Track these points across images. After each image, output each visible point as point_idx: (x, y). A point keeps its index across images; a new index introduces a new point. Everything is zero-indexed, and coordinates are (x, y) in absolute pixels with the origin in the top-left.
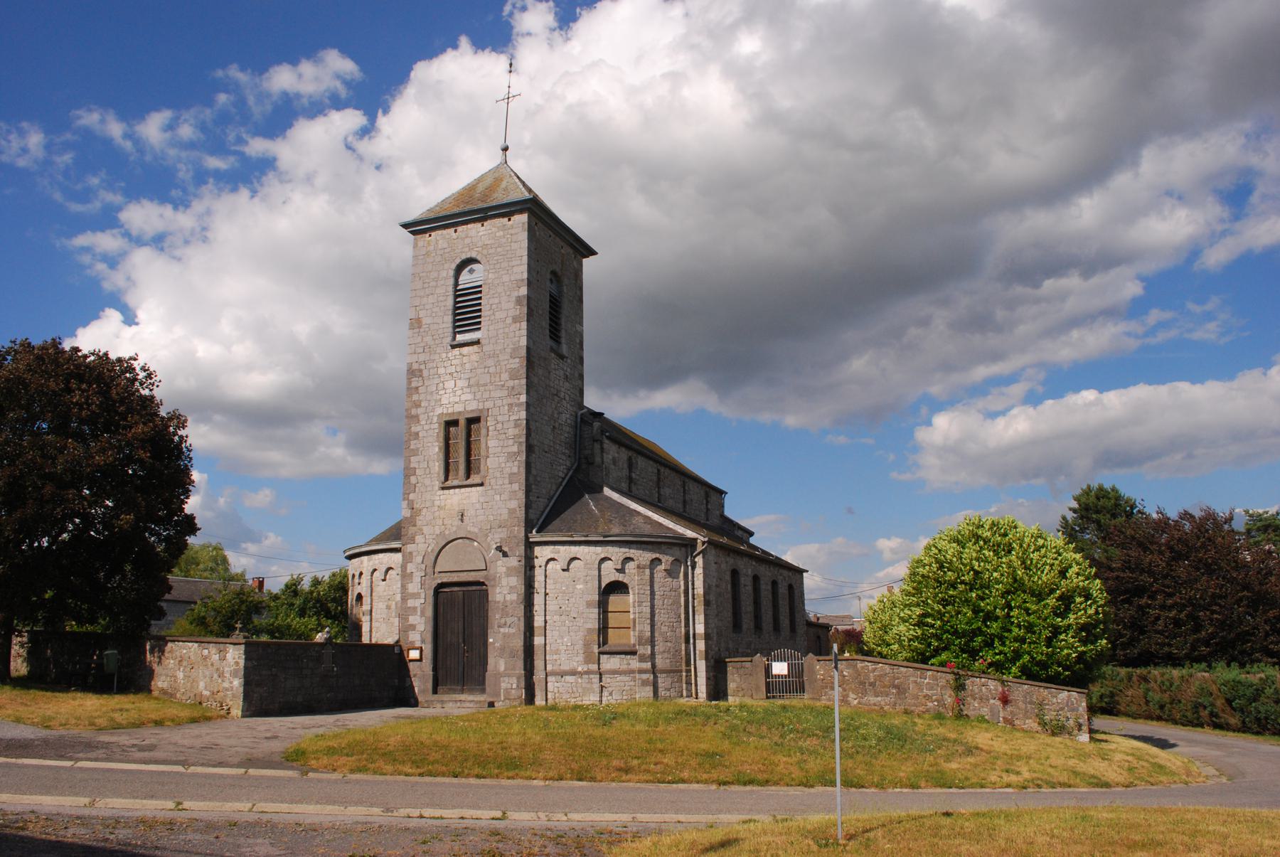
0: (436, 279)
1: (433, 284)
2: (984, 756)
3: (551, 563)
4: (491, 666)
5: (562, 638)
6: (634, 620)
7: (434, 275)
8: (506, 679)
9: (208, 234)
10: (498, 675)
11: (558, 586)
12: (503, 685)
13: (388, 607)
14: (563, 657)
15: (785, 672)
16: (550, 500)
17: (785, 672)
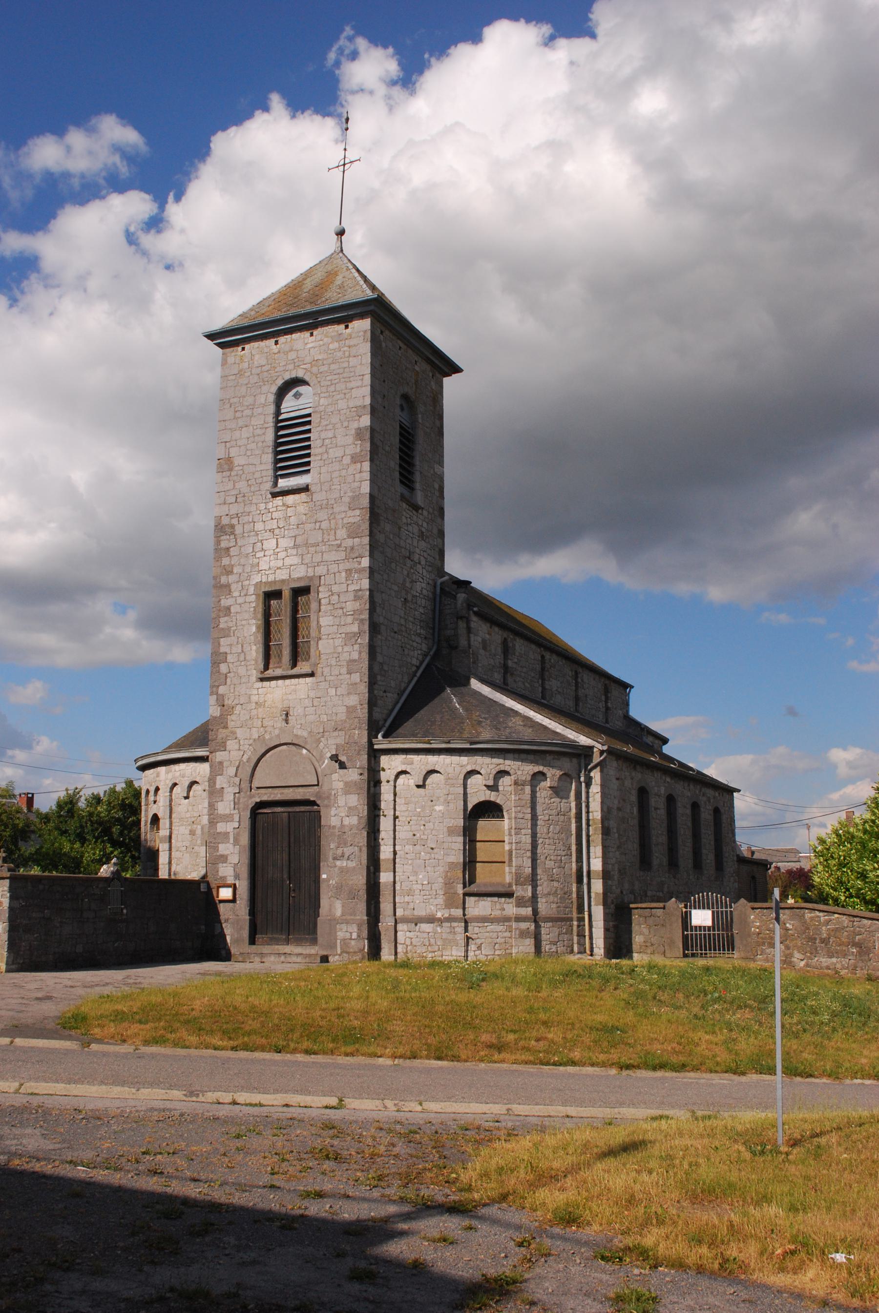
1: (248, 412)
5: (416, 873)
6: (510, 852)
7: (249, 400)
8: (344, 926)
11: (411, 807)
12: (340, 935)
13: (192, 833)
15: (709, 923)
17: (709, 923)
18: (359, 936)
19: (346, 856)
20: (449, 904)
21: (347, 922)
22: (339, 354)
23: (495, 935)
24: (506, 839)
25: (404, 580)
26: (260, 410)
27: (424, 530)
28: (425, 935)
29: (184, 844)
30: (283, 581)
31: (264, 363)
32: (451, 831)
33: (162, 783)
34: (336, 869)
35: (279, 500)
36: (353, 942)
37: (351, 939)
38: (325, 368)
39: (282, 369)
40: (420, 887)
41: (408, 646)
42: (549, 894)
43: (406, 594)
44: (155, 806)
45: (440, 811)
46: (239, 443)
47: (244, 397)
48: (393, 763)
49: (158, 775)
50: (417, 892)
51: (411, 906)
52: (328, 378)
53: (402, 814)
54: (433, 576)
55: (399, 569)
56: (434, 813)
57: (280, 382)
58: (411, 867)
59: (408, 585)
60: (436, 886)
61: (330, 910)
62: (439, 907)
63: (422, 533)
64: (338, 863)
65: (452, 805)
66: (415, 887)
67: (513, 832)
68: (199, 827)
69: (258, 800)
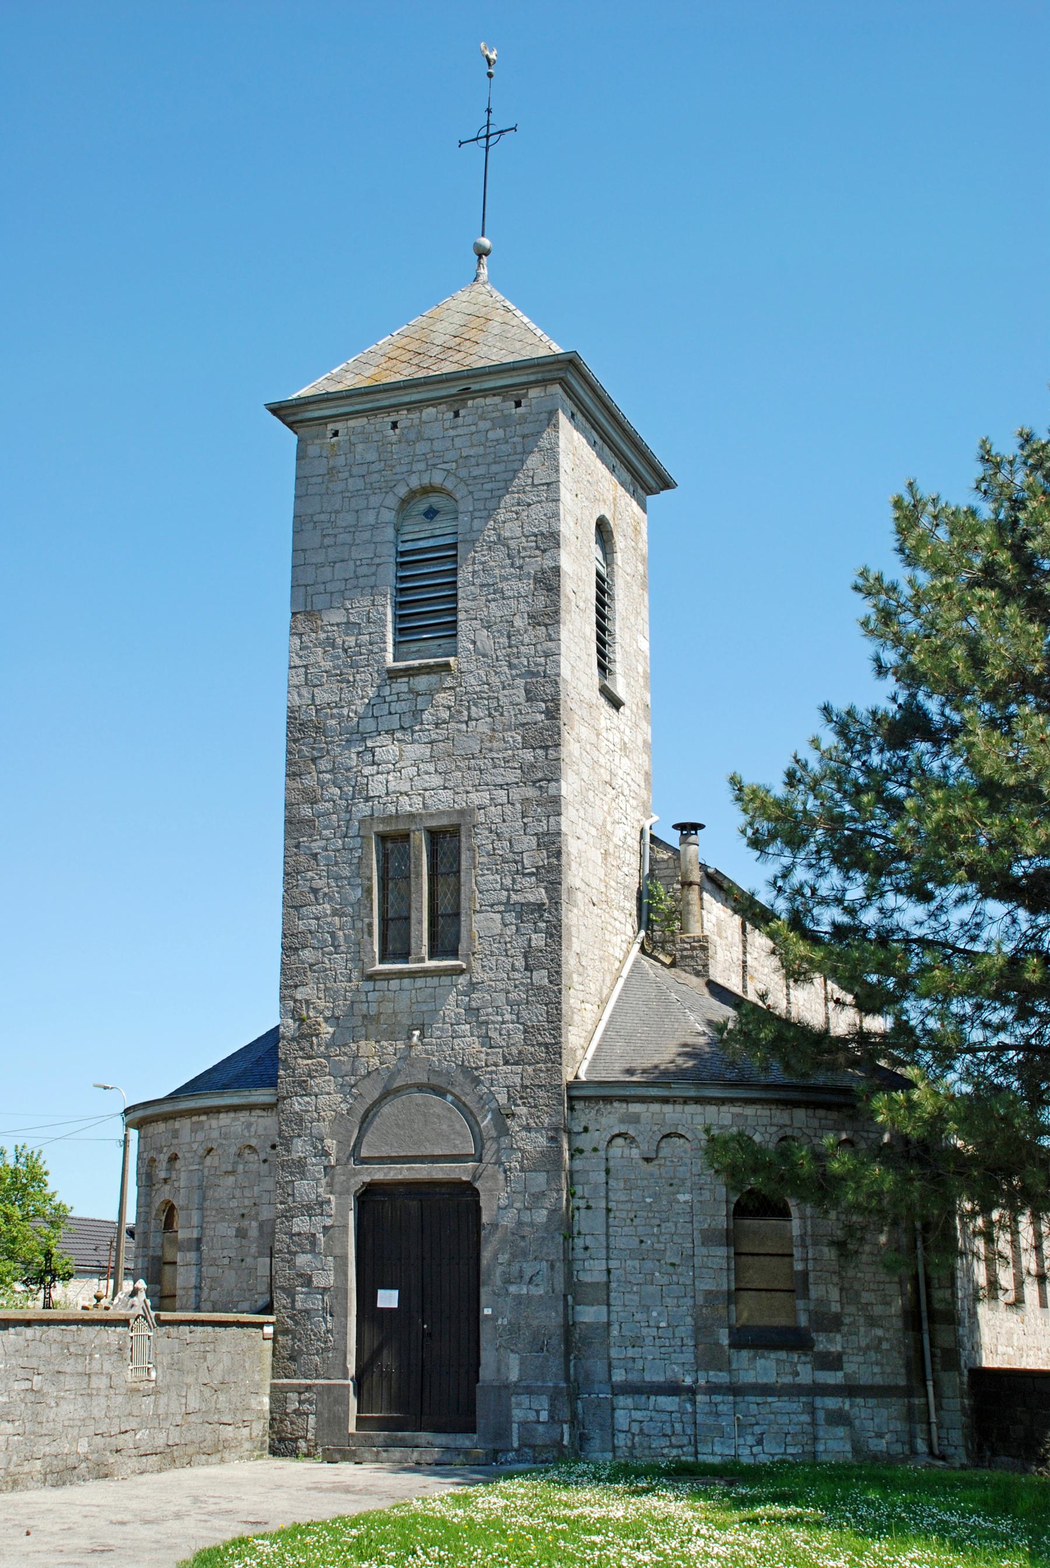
0: (353, 529)
1: (346, 538)
2: (539, 1459)
3: (620, 1141)
4: (486, 1373)
5: (647, 1309)
6: (805, 1274)
7: (349, 519)
8: (525, 1399)
9: (866, 608)
10: (505, 1389)
11: (636, 1195)
12: (518, 1414)
13: (241, 1234)
14: (650, 1352)
15: (381, 1293)
16: (603, 1003)
17: (381, 1293)
18: (551, 1417)
19: (527, 1278)
20: (701, 1364)
21: (529, 1391)
22: (505, 448)
23: (785, 1419)
24: (797, 1252)
25: (605, 821)
26: (366, 535)
27: (626, 740)
28: (665, 1417)
29: (226, 1253)
30: (411, 816)
31: (373, 459)
32: (709, 1238)
33: (185, 1148)
34: (509, 1300)
35: (401, 685)
36: (541, 1428)
37: (538, 1422)
38: (481, 470)
39: (405, 469)
40: (654, 1332)
41: (610, 928)
42: (868, 1347)
43: (607, 843)
44: (167, 1187)
45: (685, 1202)
46: (330, 587)
47: (337, 512)
48: (604, 1120)
49: (175, 1134)
50: (649, 1341)
51: (639, 1365)
52: (487, 486)
53: (620, 1206)
54: (639, 814)
55: (598, 802)
56: (676, 1206)
57: (402, 491)
58: (636, 1298)
59: (609, 827)
60: (681, 1332)
61: (499, 1370)
62: (687, 1367)
63: (625, 744)
64: (513, 1289)
65: (707, 1195)
66: (645, 1331)
67: (809, 1241)
68: (254, 1224)
69: (368, 1179)
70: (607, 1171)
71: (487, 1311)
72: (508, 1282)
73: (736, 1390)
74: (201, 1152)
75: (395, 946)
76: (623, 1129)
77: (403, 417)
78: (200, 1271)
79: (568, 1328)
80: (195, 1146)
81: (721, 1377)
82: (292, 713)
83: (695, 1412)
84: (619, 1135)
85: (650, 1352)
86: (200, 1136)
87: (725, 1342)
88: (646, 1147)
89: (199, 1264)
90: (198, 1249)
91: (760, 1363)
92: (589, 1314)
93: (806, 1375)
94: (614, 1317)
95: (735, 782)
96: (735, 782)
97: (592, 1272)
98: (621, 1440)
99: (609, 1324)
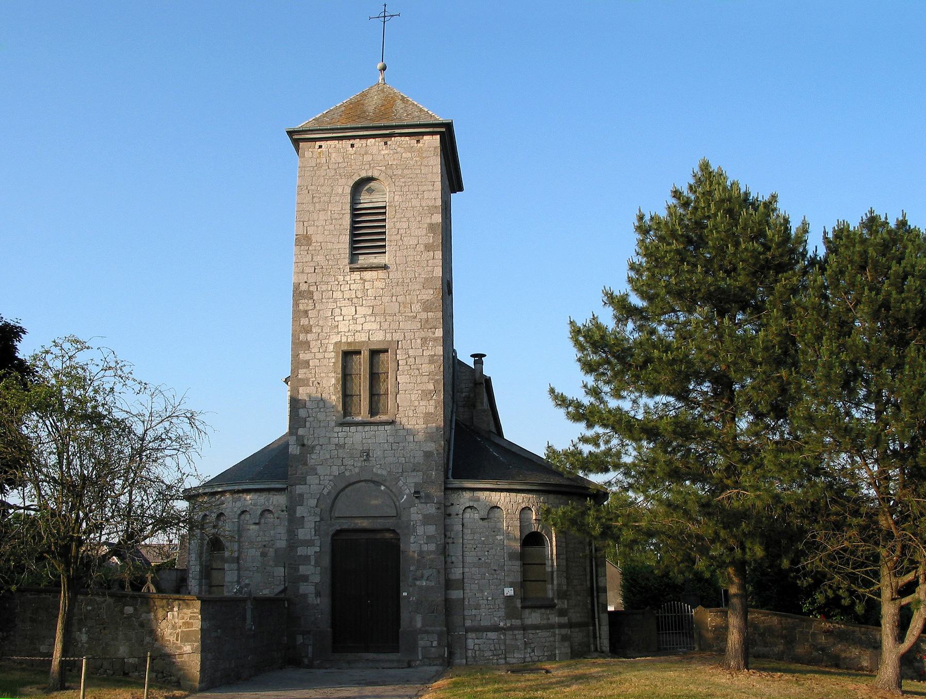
3: (469, 510)
5: (482, 591)
12: (421, 643)
13: (264, 555)
18: (439, 644)
19: (425, 578)
21: (427, 632)
36: (433, 649)
50: (483, 606)
52: (403, 180)
64: (418, 583)
66: (481, 602)
70: (463, 525)
71: (405, 594)
72: (416, 579)
73: (524, 628)
74: (239, 512)
75: (658, 630)
76: (471, 504)
77: (357, 142)
78: (239, 573)
79: (447, 600)
80: (235, 509)
81: (517, 622)
82: (297, 287)
83: (505, 639)
84: (469, 507)
85: (483, 612)
86: (239, 504)
87: (519, 606)
88: (483, 513)
89: (239, 570)
90: (238, 562)
91: (533, 614)
92: (455, 594)
93: (555, 619)
94: (466, 595)
95: (552, 391)
96: (552, 391)
97: (456, 574)
98: (470, 653)
99: (464, 599)
